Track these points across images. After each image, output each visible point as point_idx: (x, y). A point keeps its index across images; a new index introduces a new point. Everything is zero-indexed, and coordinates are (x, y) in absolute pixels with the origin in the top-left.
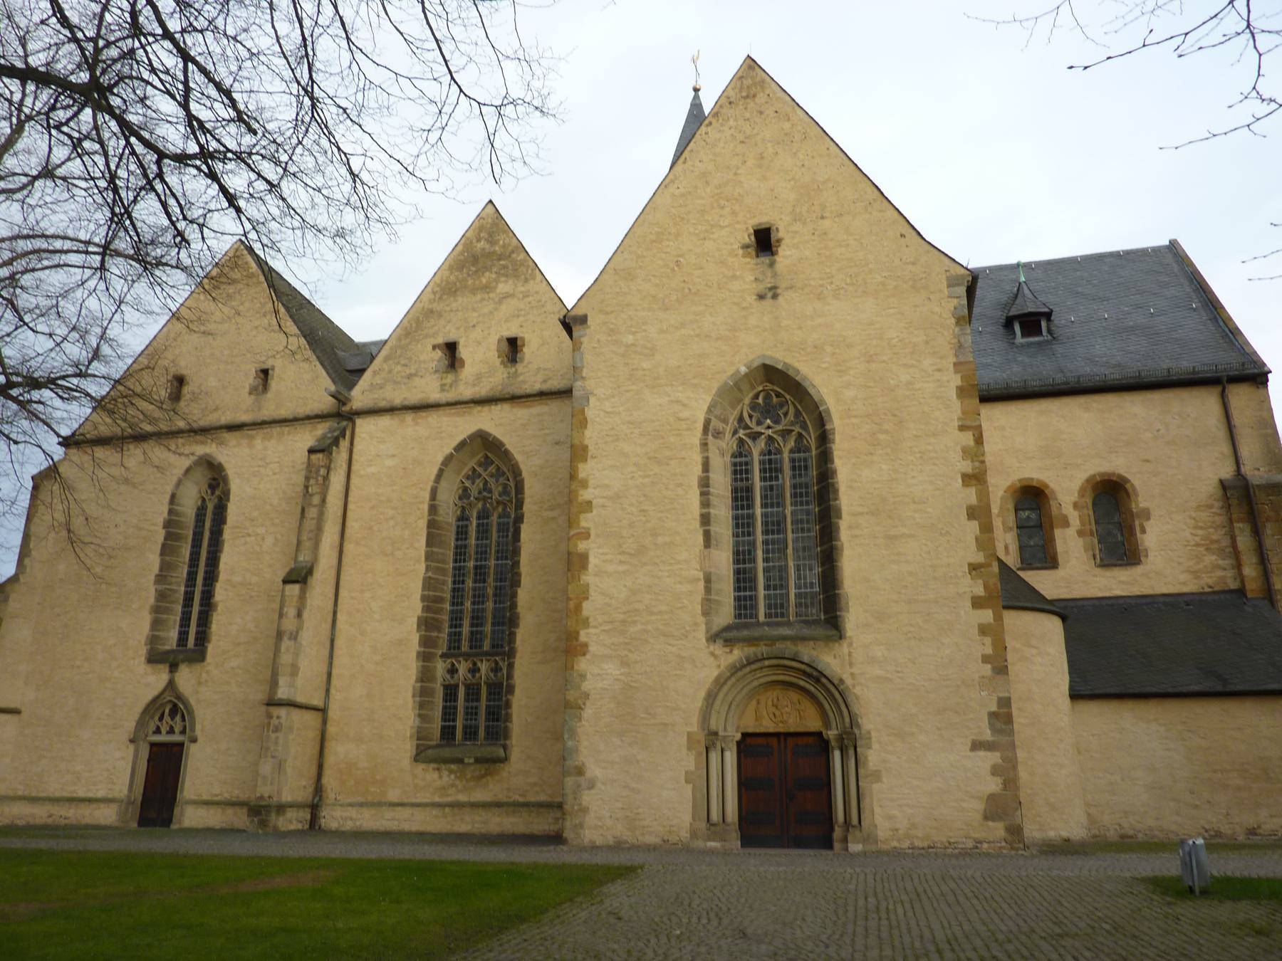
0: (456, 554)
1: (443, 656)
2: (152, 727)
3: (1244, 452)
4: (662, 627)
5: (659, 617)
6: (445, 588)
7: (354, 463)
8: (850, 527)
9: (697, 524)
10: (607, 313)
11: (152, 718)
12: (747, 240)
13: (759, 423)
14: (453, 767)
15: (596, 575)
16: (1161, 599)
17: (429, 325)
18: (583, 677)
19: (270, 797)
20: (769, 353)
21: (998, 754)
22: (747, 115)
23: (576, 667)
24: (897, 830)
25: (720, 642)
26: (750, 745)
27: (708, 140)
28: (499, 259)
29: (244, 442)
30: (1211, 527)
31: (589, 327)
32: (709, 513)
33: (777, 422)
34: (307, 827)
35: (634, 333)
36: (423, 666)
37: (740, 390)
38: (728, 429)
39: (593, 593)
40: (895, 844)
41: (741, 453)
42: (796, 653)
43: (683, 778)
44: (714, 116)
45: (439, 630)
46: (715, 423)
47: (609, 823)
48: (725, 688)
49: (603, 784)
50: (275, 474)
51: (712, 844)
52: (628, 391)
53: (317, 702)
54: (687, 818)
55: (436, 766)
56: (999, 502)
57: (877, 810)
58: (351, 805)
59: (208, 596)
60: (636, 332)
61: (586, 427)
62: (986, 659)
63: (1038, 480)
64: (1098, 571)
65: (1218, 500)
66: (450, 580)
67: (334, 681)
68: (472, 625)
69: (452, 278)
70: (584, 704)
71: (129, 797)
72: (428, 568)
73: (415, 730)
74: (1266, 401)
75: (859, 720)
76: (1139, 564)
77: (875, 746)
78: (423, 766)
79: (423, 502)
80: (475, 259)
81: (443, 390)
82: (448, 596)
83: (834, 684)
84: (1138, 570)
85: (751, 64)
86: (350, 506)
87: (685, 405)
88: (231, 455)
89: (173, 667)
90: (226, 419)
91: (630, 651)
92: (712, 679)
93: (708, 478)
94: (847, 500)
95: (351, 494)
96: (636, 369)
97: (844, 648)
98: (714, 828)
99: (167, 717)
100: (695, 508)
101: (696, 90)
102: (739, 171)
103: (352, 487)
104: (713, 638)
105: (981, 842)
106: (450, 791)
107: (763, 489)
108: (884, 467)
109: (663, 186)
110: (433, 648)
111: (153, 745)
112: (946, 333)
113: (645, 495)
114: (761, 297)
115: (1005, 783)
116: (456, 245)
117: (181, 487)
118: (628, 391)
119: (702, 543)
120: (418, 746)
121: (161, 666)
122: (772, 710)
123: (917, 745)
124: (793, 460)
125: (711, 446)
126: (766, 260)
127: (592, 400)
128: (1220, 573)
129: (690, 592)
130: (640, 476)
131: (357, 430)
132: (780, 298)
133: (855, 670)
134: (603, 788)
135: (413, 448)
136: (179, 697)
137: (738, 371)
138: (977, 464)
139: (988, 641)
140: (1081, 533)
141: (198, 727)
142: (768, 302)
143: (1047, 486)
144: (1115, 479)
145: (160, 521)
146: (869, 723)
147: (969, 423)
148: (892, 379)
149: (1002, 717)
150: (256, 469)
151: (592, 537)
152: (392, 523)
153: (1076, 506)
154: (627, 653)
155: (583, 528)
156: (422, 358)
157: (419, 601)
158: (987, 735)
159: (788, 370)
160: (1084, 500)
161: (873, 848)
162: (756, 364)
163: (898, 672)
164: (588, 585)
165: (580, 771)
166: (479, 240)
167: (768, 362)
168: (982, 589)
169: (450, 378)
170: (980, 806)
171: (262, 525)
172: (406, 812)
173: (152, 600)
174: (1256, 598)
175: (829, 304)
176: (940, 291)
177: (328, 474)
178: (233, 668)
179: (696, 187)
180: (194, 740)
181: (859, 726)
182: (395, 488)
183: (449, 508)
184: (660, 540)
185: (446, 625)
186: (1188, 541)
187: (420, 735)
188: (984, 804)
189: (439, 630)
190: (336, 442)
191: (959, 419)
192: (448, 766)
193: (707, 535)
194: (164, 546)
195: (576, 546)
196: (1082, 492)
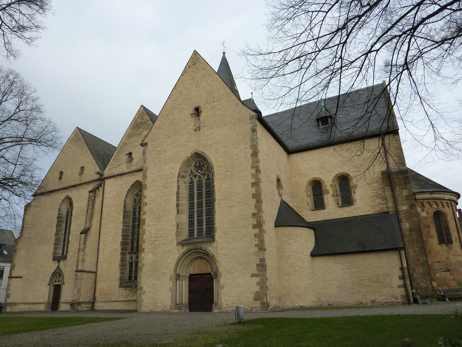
0: (133, 220)
1: (129, 253)
2: (54, 281)
4: (164, 241)
5: (164, 238)
6: (129, 231)
8: (218, 204)
9: (175, 207)
10: (153, 141)
11: (54, 277)
12: (192, 112)
13: (197, 172)
14: (129, 289)
15: (147, 226)
16: (360, 217)
17: (124, 148)
18: (143, 259)
19: (76, 300)
20: (197, 149)
21: (259, 278)
22: (194, 70)
23: (141, 256)
24: (228, 305)
25: (180, 245)
26: (192, 278)
27: (183, 81)
28: (144, 124)
29: (77, 190)
30: (378, 189)
31: (148, 146)
32: (178, 203)
33: (202, 171)
35: (160, 147)
36: (122, 257)
37: (190, 162)
38: (188, 175)
39: (146, 232)
40: (227, 309)
41: (192, 182)
43: (169, 290)
44: (184, 72)
45: (128, 245)
47: (149, 305)
48: (182, 260)
49: (147, 292)
50: (84, 200)
51: (176, 311)
52: (158, 166)
53: (93, 270)
54: (169, 303)
55: (125, 288)
56: (305, 187)
58: (102, 302)
60: (161, 146)
61: (146, 179)
62: (256, 246)
63: (318, 178)
64: (339, 209)
65: (381, 179)
66: (131, 229)
67: (99, 263)
69: (131, 132)
70: (143, 267)
71: (48, 302)
72: (123, 226)
73: (119, 277)
76: (353, 205)
77: (223, 277)
79: (122, 205)
80: (137, 125)
81: (128, 168)
82: (131, 234)
84: (353, 207)
85: (195, 53)
86: (104, 208)
87: (173, 169)
88: (74, 194)
89: (59, 261)
90: (73, 184)
91: (155, 250)
93: (178, 192)
94: (218, 195)
96: (161, 158)
97: (214, 245)
98: (178, 306)
99: (58, 277)
101: (224, 53)
102: (191, 90)
104: (178, 244)
105: (253, 308)
106: (128, 297)
107: (198, 193)
109: (169, 98)
110: (126, 251)
111: (55, 285)
112: (248, 136)
114: (195, 130)
116: (132, 121)
117: (61, 206)
118: (158, 166)
119: (176, 213)
120: (120, 282)
121: (56, 261)
122: (198, 266)
123: (235, 276)
124: (206, 183)
125: (180, 181)
126: (197, 118)
127: (148, 170)
128: (382, 206)
129: (173, 229)
130: (160, 193)
131: (105, 183)
132: (201, 130)
133: (218, 252)
134: (147, 294)
135: (120, 188)
136: (60, 271)
137: (188, 156)
138: (256, 179)
139: (257, 239)
140: (333, 196)
141: (65, 279)
142: (197, 132)
143: (321, 180)
144: (345, 175)
145: (56, 217)
146: (221, 270)
147: (254, 166)
148: (232, 153)
149: (262, 266)
150: (80, 199)
151: (147, 214)
152: (114, 212)
153: (331, 186)
154: (155, 250)
155: (145, 211)
156: (122, 159)
157: (121, 236)
158: (256, 272)
159: (202, 153)
160: (334, 183)
161: (221, 311)
162: (193, 153)
163: (230, 252)
164: (145, 229)
165: (141, 289)
166: (138, 119)
167: (197, 152)
168: (256, 222)
169: (130, 164)
170: (253, 296)
171: (81, 216)
172: (116, 304)
173: (54, 241)
175: (215, 130)
176: (247, 122)
177: (94, 199)
178: (74, 261)
179: (179, 96)
180: (64, 284)
182: (115, 201)
183: (130, 206)
184: (165, 213)
186: (370, 195)
187: (121, 279)
188: (254, 295)
189: (128, 245)
190: (98, 188)
191: (251, 164)
192: (128, 288)
193: (178, 210)
194: (57, 224)
195: (142, 217)
196: (333, 181)
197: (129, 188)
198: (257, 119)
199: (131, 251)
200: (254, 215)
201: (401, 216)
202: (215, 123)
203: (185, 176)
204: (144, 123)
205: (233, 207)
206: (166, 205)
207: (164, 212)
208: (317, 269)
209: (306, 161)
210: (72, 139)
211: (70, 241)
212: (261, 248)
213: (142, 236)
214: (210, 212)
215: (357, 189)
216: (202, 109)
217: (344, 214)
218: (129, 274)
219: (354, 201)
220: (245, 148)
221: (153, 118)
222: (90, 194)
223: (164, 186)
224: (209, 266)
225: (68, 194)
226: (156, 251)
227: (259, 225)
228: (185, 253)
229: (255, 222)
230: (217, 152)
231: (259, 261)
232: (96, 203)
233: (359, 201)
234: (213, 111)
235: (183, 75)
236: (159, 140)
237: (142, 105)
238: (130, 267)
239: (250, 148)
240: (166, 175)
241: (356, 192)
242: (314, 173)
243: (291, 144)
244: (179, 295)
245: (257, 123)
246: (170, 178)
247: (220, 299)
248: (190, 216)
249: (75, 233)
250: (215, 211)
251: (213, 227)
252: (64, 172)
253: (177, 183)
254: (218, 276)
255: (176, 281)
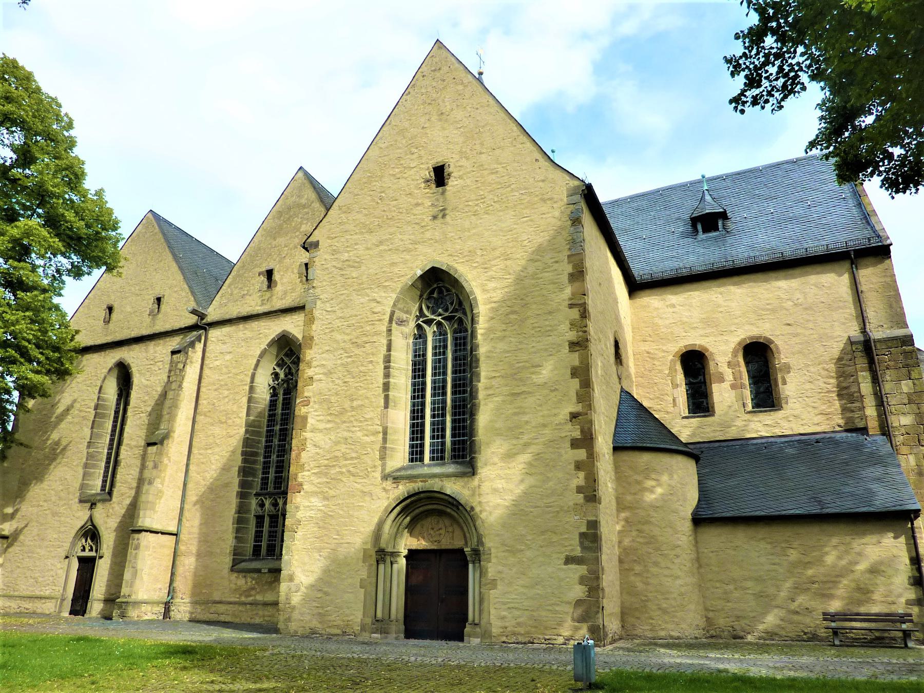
0: (269, 421)
1: (257, 495)
3: (870, 314)
4: (352, 469)
7: (206, 358)
8: (486, 388)
14: (255, 575)
16: (797, 438)
23: (294, 501)
28: (304, 208)
32: (389, 382)
33: (446, 310)
34: (161, 618)
35: (348, 252)
36: (240, 502)
40: (504, 639)
42: (442, 488)
43: (358, 584)
45: (254, 475)
46: (398, 314)
50: (160, 369)
55: (244, 574)
57: (493, 611)
59: (117, 454)
62: (579, 490)
63: (700, 346)
66: (264, 440)
68: (276, 472)
72: (247, 431)
73: (232, 549)
74: (891, 267)
75: (483, 539)
76: (780, 410)
77: (494, 560)
78: (236, 575)
79: (246, 385)
81: (263, 304)
82: (262, 451)
83: (466, 510)
84: (779, 414)
86: (203, 389)
87: (378, 302)
89: (93, 505)
92: (382, 508)
93: (389, 356)
95: (203, 381)
98: (380, 625)
100: (381, 380)
103: (204, 376)
106: (253, 592)
108: (512, 339)
109: (374, 143)
112: (563, 233)
113: (348, 371)
114: (435, 217)
115: (590, 591)
117: (106, 381)
118: (342, 294)
120: (234, 559)
123: (524, 559)
127: (319, 302)
132: (448, 217)
138: (581, 333)
139: (582, 475)
142: (439, 222)
144: (761, 341)
151: (311, 404)
152: (227, 400)
154: (327, 489)
157: (240, 456)
158: (578, 552)
165: (291, 578)
168: (579, 433)
169: (268, 294)
174: (876, 435)
176: (562, 200)
177: (184, 367)
181: (482, 544)
184: (355, 404)
185: (260, 472)
189: (254, 475)
190: (192, 344)
191: (571, 299)
192: (251, 574)
193: (387, 398)
195: (300, 410)
197: (263, 348)
198: (584, 195)
199: (261, 489)
200: (574, 416)
201: (897, 440)
202: (482, 201)
203: (404, 321)
204: (304, 206)
205: (523, 396)
206: (357, 385)
207: (352, 400)
208: (706, 551)
209: (673, 306)
210: (138, 235)
211: (123, 461)
212: (590, 494)
213: (298, 456)
214: (465, 406)
215: (791, 374)
216: (451, 170)
217: (759, 429)
218: (255, 541)
219: (783, 402)
220: (553, 260)
221: (326, 200)
222: (174, 356)
223: (355, 340)
224: (458, 532)
225: (123, 356)
226: (330, 491)
227: (586, 440)
228: (402, 498)
229: (577, 434)
230: (486, 268)
231: (585, 527)
232: (186, 377)
233: (795, 400)
234: (479, 175)
235: (409, 93)
236: (347, 237)
237: (301, 168)
238: (257, 527)
239: (566, 260)
240: (359, 317)
241: (787, 380)
242: (689, 334)
243: (639, 269)
244: (384, 600)
245: (583, 205)
246: (370, 323)
247: (485, 615)
248: (414, 413)
249: (133, 443)
250: (479, 403)
251: (473, 443)
252: (116, 306)
253: (387, 337)
254: (482, 557)
255: (378, 564)
